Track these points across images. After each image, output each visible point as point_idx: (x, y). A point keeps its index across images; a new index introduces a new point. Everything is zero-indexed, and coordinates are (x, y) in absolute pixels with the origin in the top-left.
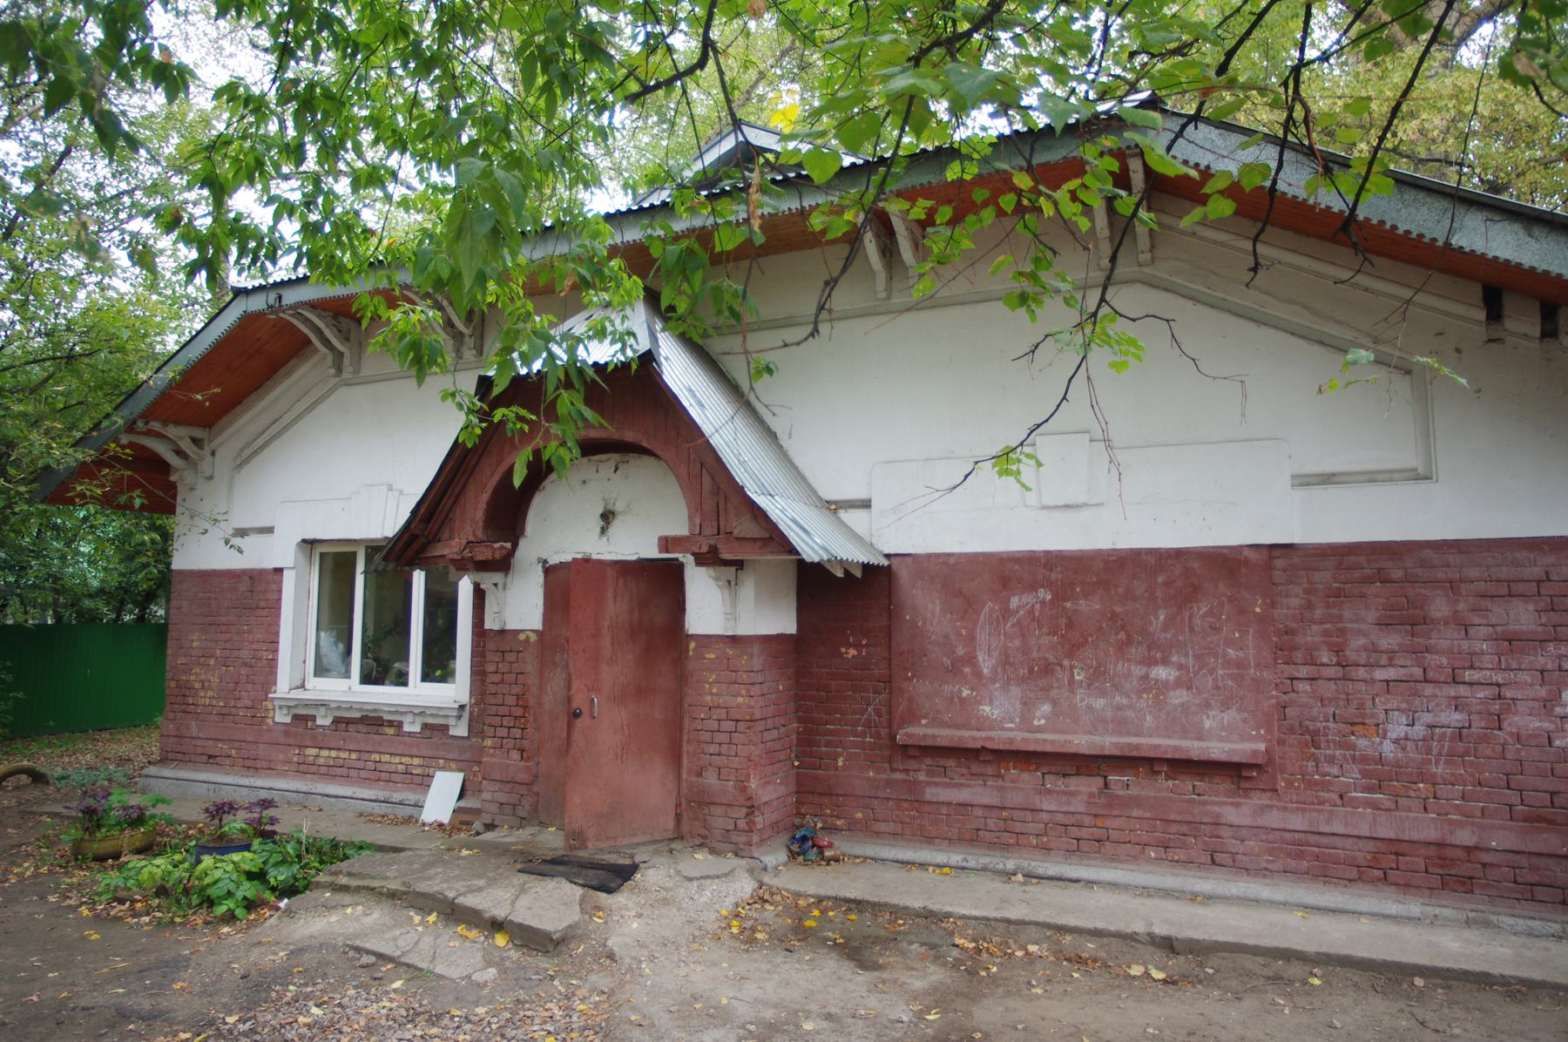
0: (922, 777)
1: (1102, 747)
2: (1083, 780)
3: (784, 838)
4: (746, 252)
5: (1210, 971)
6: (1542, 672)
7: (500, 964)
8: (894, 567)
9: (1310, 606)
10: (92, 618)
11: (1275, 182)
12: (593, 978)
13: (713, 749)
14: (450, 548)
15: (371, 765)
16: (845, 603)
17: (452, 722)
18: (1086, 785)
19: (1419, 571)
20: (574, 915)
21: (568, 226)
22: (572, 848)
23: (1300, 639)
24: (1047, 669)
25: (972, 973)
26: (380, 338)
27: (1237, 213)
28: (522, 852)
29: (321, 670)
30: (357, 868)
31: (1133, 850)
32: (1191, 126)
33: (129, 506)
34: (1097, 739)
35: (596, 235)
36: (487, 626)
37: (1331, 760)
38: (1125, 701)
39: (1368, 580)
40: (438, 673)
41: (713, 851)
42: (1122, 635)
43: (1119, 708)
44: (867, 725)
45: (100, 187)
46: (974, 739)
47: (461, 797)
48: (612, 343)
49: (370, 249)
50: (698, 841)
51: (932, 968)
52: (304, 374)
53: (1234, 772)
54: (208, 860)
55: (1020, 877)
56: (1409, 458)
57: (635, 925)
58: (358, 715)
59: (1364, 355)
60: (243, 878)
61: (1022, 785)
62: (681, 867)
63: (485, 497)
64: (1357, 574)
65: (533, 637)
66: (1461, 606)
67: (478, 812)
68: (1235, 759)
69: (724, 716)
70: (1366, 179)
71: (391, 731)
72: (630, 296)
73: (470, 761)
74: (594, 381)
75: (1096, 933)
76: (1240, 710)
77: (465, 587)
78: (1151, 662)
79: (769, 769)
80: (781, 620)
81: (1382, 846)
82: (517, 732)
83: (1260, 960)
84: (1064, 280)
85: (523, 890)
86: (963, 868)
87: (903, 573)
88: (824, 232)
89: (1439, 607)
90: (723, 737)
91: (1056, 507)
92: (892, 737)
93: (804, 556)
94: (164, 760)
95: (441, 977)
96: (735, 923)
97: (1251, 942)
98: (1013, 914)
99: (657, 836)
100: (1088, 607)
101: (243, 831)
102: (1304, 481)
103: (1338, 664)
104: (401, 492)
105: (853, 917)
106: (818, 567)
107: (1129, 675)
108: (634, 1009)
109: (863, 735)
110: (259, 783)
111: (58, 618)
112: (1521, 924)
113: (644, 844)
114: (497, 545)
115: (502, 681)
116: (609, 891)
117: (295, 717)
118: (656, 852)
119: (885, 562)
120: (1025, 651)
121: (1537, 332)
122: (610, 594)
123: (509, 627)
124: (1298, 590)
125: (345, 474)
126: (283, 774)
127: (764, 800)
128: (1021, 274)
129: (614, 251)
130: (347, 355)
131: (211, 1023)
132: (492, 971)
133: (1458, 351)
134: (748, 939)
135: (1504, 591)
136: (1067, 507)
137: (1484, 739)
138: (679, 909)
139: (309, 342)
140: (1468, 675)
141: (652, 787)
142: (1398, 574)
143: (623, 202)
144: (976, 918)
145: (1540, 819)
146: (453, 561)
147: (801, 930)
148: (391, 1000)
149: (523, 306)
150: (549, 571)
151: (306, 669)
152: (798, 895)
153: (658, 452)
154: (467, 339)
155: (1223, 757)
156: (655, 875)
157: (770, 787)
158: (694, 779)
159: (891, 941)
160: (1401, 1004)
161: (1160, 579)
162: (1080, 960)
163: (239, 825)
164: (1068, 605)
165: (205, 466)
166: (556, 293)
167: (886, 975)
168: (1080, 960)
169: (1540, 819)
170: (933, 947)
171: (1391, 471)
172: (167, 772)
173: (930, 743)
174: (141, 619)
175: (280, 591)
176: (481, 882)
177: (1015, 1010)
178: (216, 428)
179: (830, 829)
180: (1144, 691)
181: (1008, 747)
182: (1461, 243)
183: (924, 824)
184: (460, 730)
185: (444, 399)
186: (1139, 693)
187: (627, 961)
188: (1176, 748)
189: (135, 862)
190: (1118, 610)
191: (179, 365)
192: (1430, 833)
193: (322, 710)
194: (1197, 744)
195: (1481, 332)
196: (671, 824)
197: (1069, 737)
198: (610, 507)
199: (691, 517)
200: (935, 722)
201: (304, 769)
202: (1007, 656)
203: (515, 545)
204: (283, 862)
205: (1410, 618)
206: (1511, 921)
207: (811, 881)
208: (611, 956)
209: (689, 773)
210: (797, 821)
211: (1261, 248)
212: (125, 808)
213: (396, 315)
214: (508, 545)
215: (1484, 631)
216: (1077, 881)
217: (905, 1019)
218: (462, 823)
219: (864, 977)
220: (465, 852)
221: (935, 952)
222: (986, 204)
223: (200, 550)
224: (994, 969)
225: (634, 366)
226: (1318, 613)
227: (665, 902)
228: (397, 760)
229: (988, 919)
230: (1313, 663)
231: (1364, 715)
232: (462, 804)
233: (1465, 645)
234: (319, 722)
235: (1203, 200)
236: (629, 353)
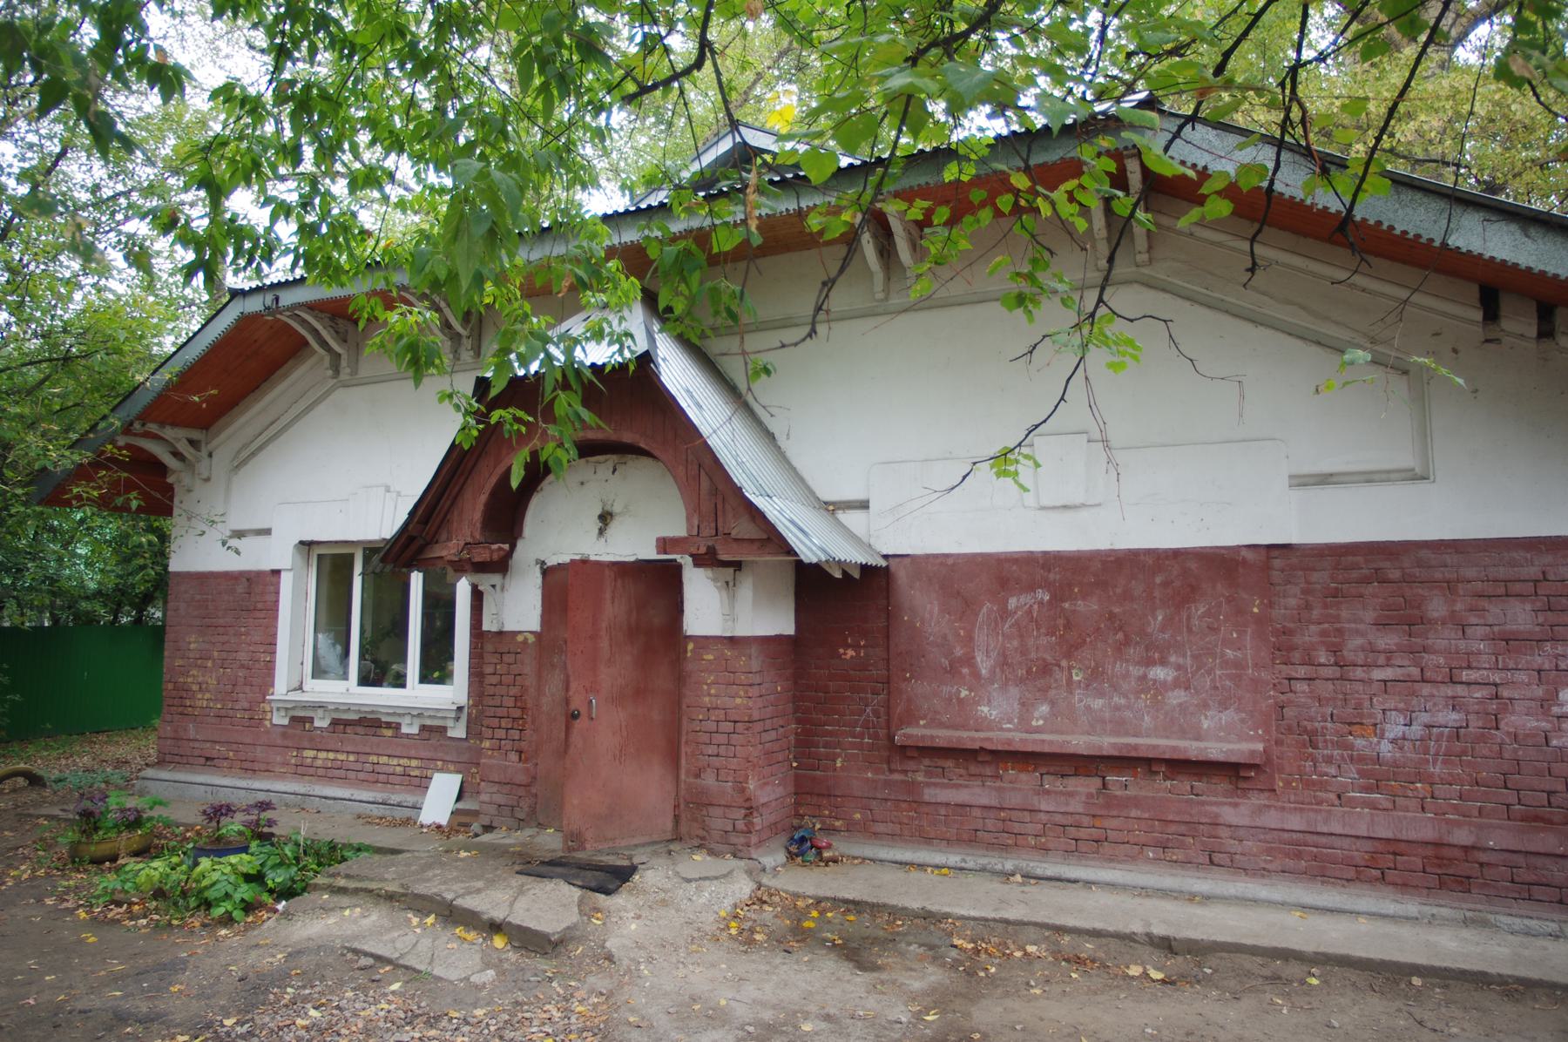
0: (920, 778)
1: (1101, 748)
2: (1082, 780)
3: (783, 839)
4: (743, 253)
5: (1209, 971)
6: (1539, 672)
7: (498, 966)
8: (893, 569)
9: (1308, 607)
10: (90, 620)
11: (1272, 182)
12: (591, 979)
13: (711, 750)
14: (448, 550)
15: (368, 767)
16: (843, 603)
17: (450, 723)
18: (1084, 786)
19: (1417, 571)
20: (572, 917)
21: (566, 227)
22: (570, 849)
23: (1297, 640)
24: (1046, 669)
25: (970, 973)
26: (377, 340)
27: (1234, 213)
28: (520, 854)
29: (319, 672)
30: (355, 870)
31: (1132, 850)
32: (1189, 127)
33: (125, 508)
34: (1095, 739)
35: (594, 236)
36: (485, 628)
37: (1329, 760)
38: (1123, 701)
39: (1366, 581)
40: (436, 674)
41: (711, 852)
42: (1120, 636)
43: (1117, 708)
44: (866, 725)
45: (96, 188)
46: (973, 739)
47: (459, 798)
48: (610, 344)
49: (367, 250)
50: (696, 842)
51: (931, 969)
52: (302, 375)
53: (1232, 772)
54: (205, 863)
55: (1018, 878)
56: (1405, 458)
57: (633, 927)
58: (355, 717)
59: (1361, 355)
60: (241, 880)
61: (1020, 786)
62: (680, 868)
63: (483, 498)
64: (1355, 574)
65: (531, 639)
66: (1459, 606)
67: (475, 814)
68: (1233, 759)
69: (722, 717)
70: (1363, 179)
71: (389, 733)
72: (627, 297)
73: (467, 762)
74: (591, 382)
75: (1095, 934)
76: (1238, 710)
77: (463, 589)
78: (1150, 663)
79: (767, 770)
80: (779, 622)
81: (1380, 846)
82: (515, 734)
83: (1259, 960)
84: (1061, 281)
85: (521, 891)
86: (961, 869)
87: (901, 575)
88: (821, 233)
89: (1436, 607)
90: (722, 739)
91: (1054, 508)
92: (891, 738)
93: (802, 557)
94: (161, 763)
95: (439, 979)
96: (733, 924)
97: (1249, 942)
98: (1011, 914)
99: (655, 837)
100: (1087, 607)
101: (240, 833)
102: (1302, 481)
103: (1336, 664)
104: (399, 494)
105: (852, 918)
106: (816, 567)
107: (1126, 676)
108: (632, 1011)
109: (862, 736)
110: (257, 785)
111: (55, 620)
112: (1518, 923)
113: (643, 845)
114: (495, 547)
115: (500, 683)
116: (608, 892)
117: (293, 719)
118: (655, 854)
119: (883, 563)
120: (1024, 652)
121: (1533, 332)
122: (608, 595)
123: (507, 628)
124: (1296, 590)
125: (342, 475)
126: (282, 776)
127: (763, 800)
128: (1018, 274)
129: (611, 252)
130: (344, 357)
131: (209, 1025)
132: (491, 973)
133: (1455, 351)
134: (746, 940)
135: (1501, 591)
136: (1065, 507)
137: (1481, 739)
138: (678, 910)
139: (307, 343)
140: (1465, 675)
141: (650, 788)
142: (1395, 574)
143: (621, 203)
144: (975, 919)
145: (1537, 818)
146: (451, 562)
147: (798, 932)
148: (389, 1002)
149: (521, 307)
150: (547, 572)
151: (304, 671)
152: (796, 896)
153: (656, 453)
154: (465, 341)
155: (1221, 758)
156: (653, 876)
157: (769, 788)
158: (692, 780)
159: (889, 942)
160: (1399, 1004)
161: (1158, 580)
162: (1079, 961)
163: (237, 827)
164: (1067, 605)
165: (203, 468)
166: (553, 294)
167: (884, 976)
168: (1079, 961)
169: (1537, 818)
170: (931, 947)
171: (1388, 472)
172: (164, 775)
173: (928, 743)
174: (138, 621)
175: (277, 593)
176: (480, 884)
177: (1014, 1011)
178: (214, 429)
179: (829, 830)
180: (1142, 691)
181: (1006, 748)
182: (1460, 243)
183: (922, 824)
184: (458, 731)
185: (441, 400)
186: (1138, 693)
187: (626, 962)
188: (1174, 748)
189: (132, 864)
190: (1116, 610)
191: (176, 367)
192: (1428, 833)
193: (320, 712)
194: (1195, 744)
195: (1478, 332)
196: (669, 825)
197: (1068, 738)
198: (608, 508)
199: (689, 519)
200: (935, 723)
201: (302, 770)
202: (1005, 656)
203: (513, 547)
204: (281, 864)
205: (1409, 619)
206: (1509, 920)
207: (809, 882)
208: (609, 958)
209: (688, 772)
210: (796, 822)
211: (1258, 249)
212: (122, 811)
213: (393, 317)
214: (506, 547)
215: (1481, 631)
216: (1075, 881)
217: (904, 1019)
218: (460, 825)
219: (863, 978)
220: (463, 854)
221: (934, 953)
222: (983, 204)
223: (197, 552)
224: (993, 970)
225: (632, 368)
226: (1316, 613)
227: (664, 903)
228: (395, 761)
229: (986, 920)
230: (1310, 662)
231: (1362, 716)
232: (461, 805)
233: (1462, 644)
234: (317, 723)
235: (1201, 201)
236: (627, 354)
